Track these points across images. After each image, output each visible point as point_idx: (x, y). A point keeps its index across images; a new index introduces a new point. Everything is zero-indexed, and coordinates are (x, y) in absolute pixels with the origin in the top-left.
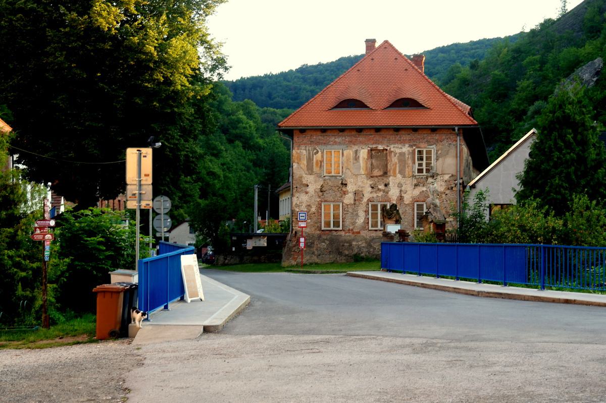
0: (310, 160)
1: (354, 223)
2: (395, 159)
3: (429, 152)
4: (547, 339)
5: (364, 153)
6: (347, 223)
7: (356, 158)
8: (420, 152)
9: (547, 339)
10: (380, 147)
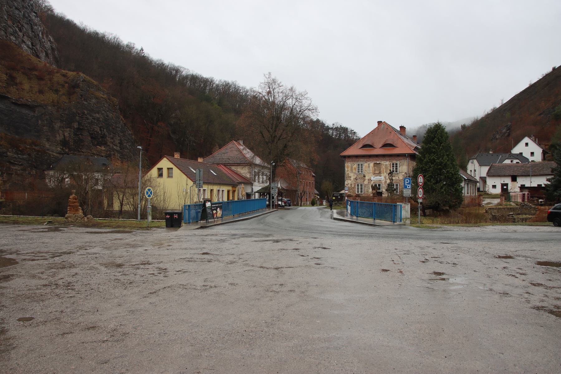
0: (352, 167)
1: (368, 191)
2: (384, 167)
3: (396, 164)
4: (347, 228)
5: (372, 165)
6: (365, 191)
7: (369, 167)
8: (393, 164)
9: (347, 228)
10: (378, 162)
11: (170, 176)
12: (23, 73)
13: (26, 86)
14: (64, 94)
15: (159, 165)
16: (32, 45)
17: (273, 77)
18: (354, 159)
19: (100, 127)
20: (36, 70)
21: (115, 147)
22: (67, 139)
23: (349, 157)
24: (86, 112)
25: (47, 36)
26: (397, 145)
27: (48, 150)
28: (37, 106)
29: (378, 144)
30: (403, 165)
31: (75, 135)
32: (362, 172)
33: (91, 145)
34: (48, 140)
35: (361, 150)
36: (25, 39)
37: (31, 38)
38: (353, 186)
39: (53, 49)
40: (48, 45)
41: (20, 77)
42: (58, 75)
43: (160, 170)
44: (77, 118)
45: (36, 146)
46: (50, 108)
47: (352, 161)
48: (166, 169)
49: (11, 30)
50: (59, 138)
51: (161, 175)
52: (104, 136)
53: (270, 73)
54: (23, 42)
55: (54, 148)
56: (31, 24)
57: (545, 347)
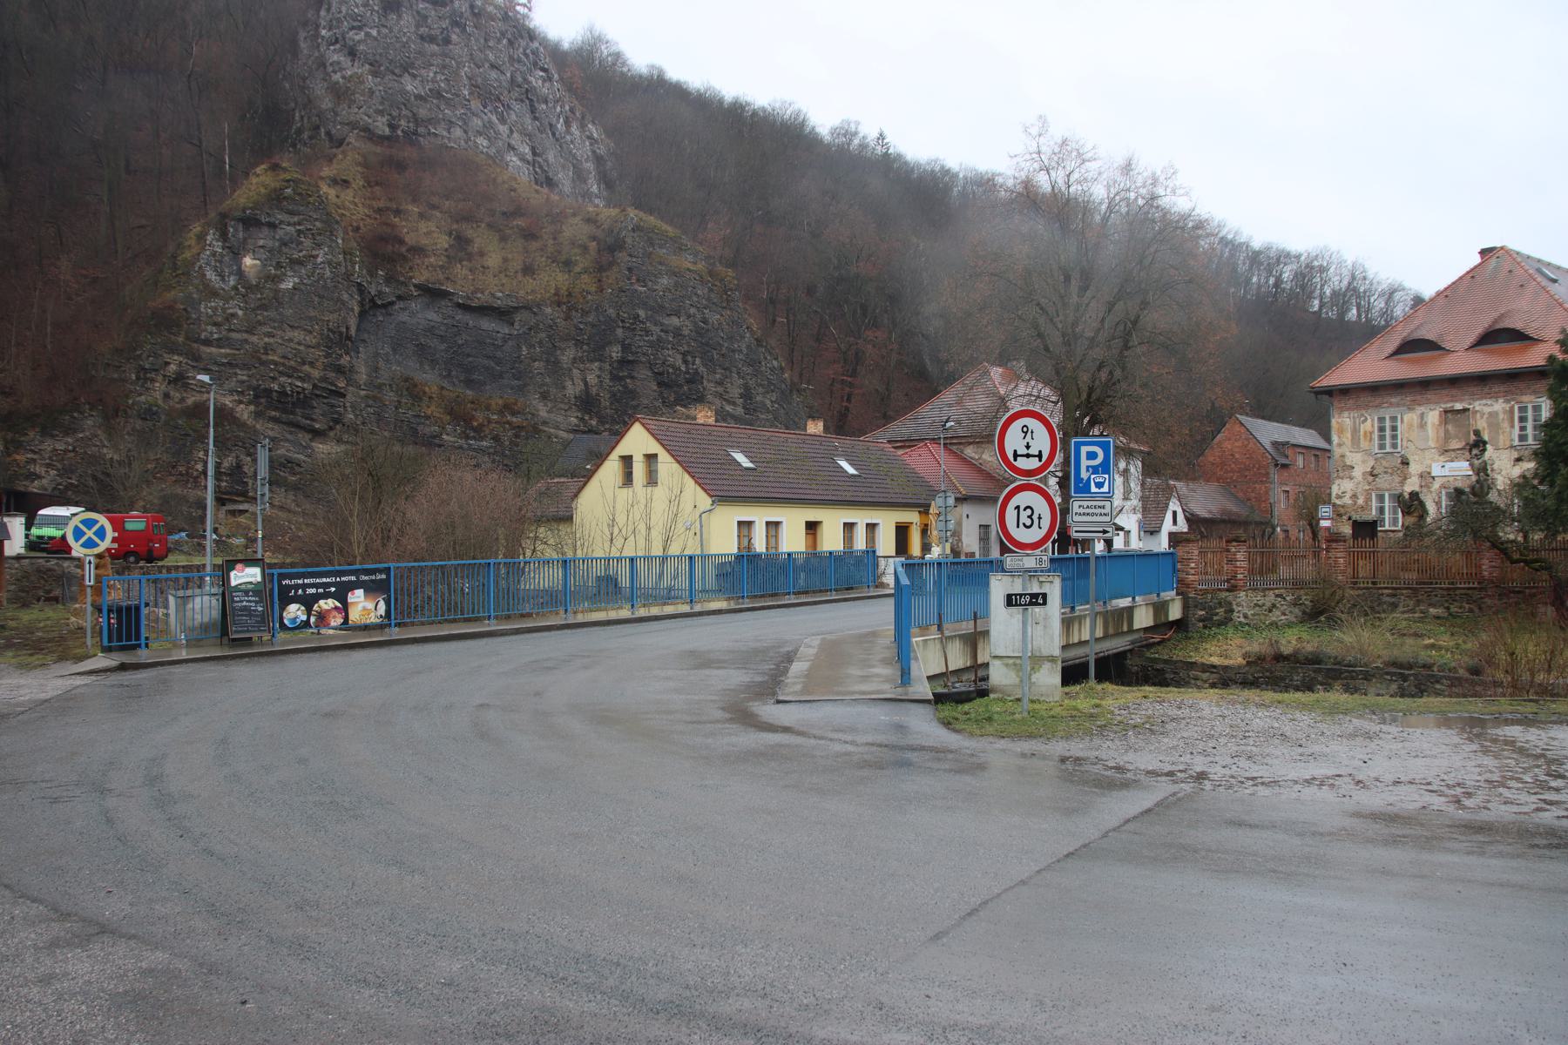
0: (1355, 431)
5: (1433, 416)
7: (1422, 425)
8: (1523, 409)
10: (1458, 406)
11: (652, 480)
12: (489, 226)
13: (493, 260)
14: (586, 271)
15: (623, 448)
16: (534, 154)
17: (1057, 133)
18: (1365, 398)
19: (684, 354)
20: (522, 215)
21: (729, 408)
22: (594, 391)
23: (1345, 391)
24: (642, 313)
25: (583, 127)
27: (545, 423)
28: (517, 309)
29: (1458, 334)
31: (615, 378)
32: (1394, 446)
33: (658, 404)
34: (544, 397)
35: (1392, 364)
36: (516, 139)
37: (530, 136)
38: (1361, 501)
39: (599, 160)
40: (583, 150)
41: (481, 238)
42: (576, 220)
43: (627, 460)
44: (619, 332)
45: (513, 414)
46: (549, 310)
47: (1358, 408)
48: (641, 458)
49: (477, 122)
50: (573, 389)
51: (628, 478)
52: (694, 379)
53: (1042, 119)
54: (511, 147)
55: (560, 419)
56: (529, 97)
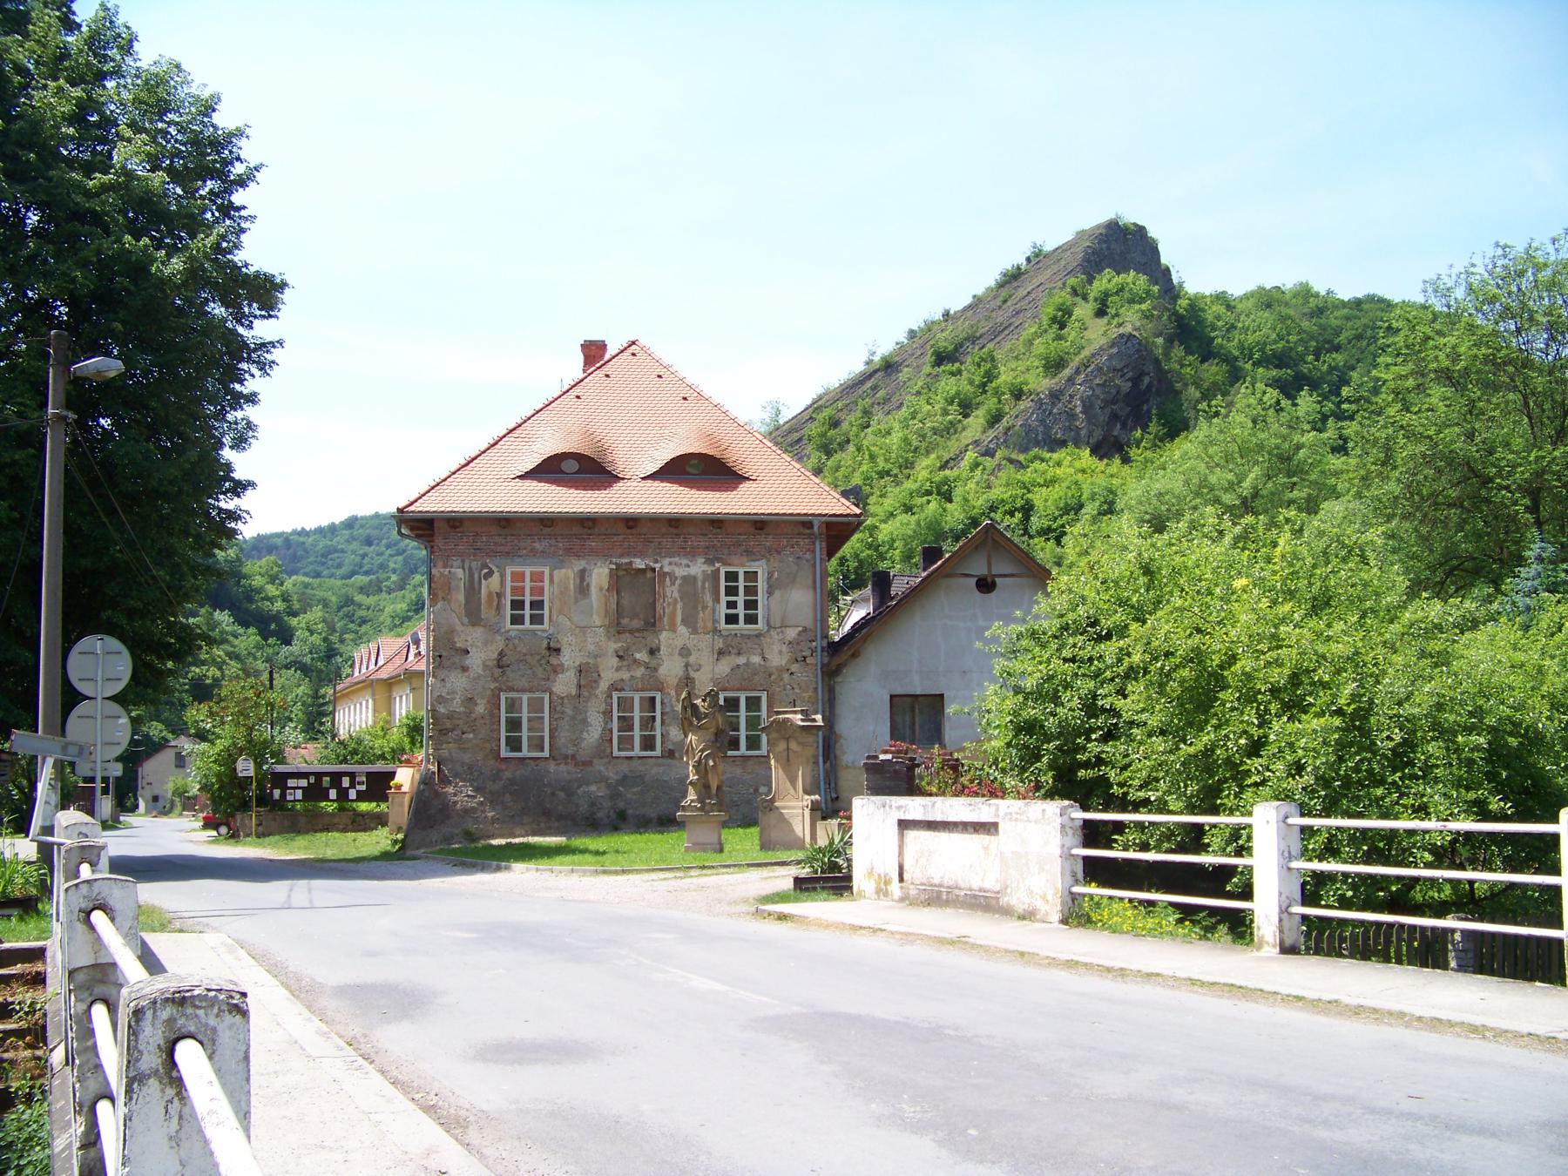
0: (472, 590)
2: (672, 591)
3: (751, 576)
7: (583, 589)
8: (731, 576)
10: (639, 563)
26: (746, 469)
30: (790, 581)
38: (481, 709)
57: (369, 542)
